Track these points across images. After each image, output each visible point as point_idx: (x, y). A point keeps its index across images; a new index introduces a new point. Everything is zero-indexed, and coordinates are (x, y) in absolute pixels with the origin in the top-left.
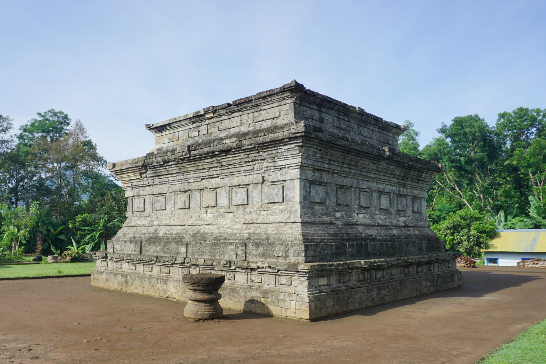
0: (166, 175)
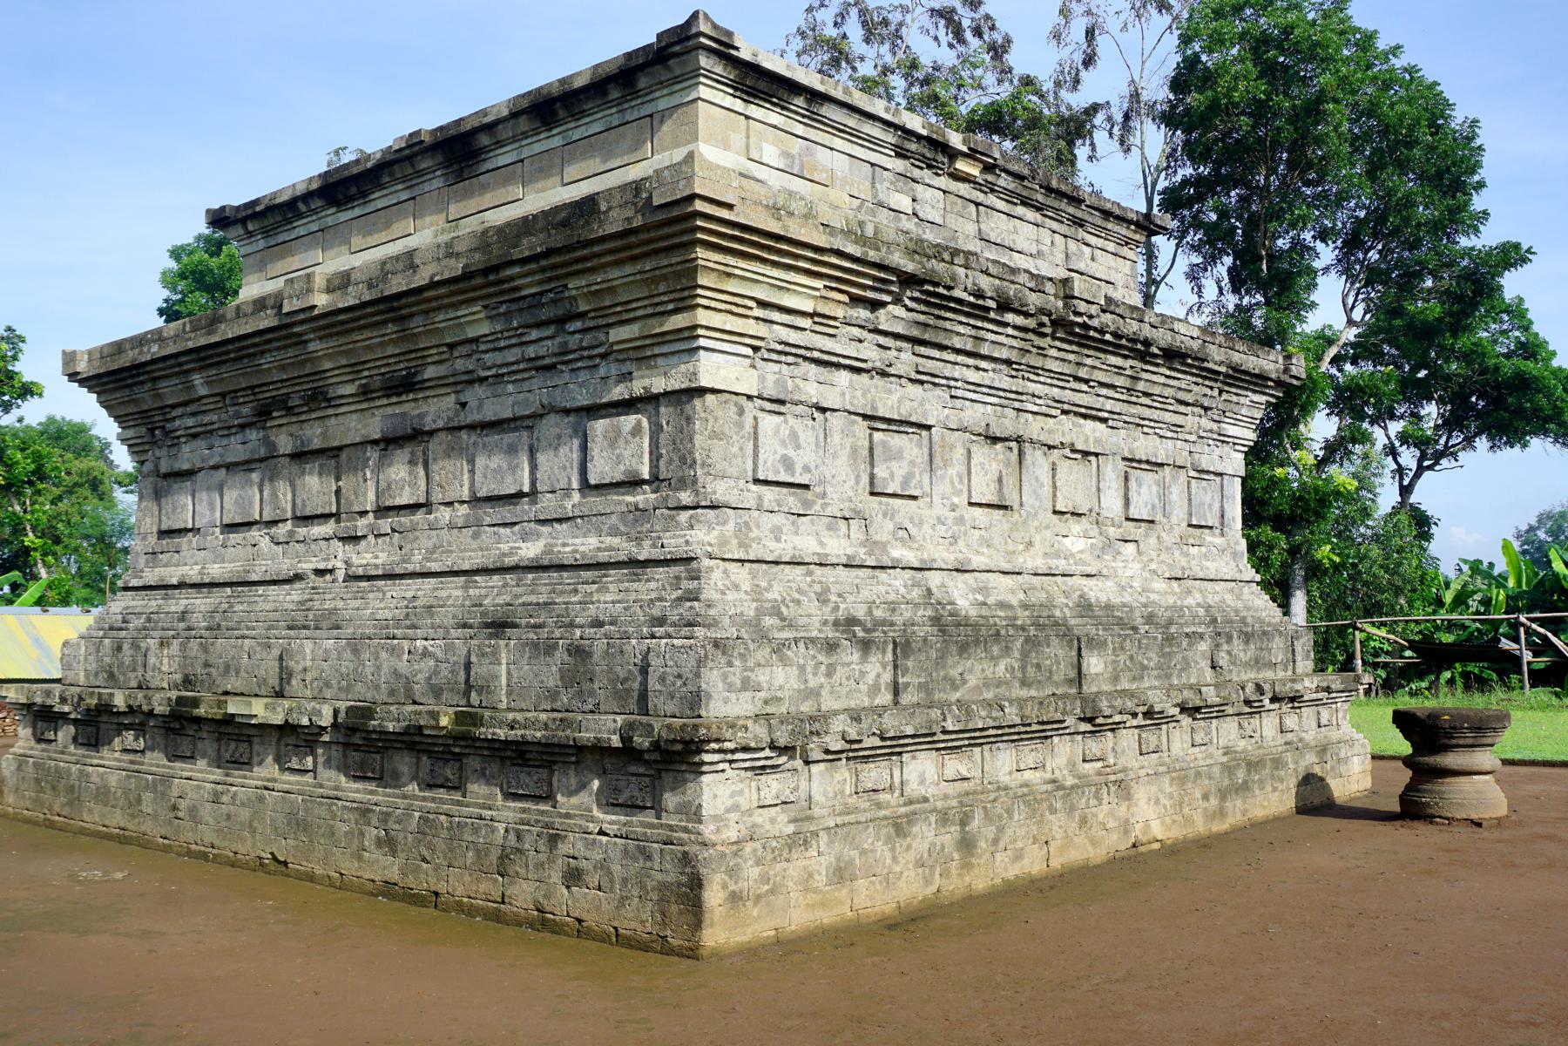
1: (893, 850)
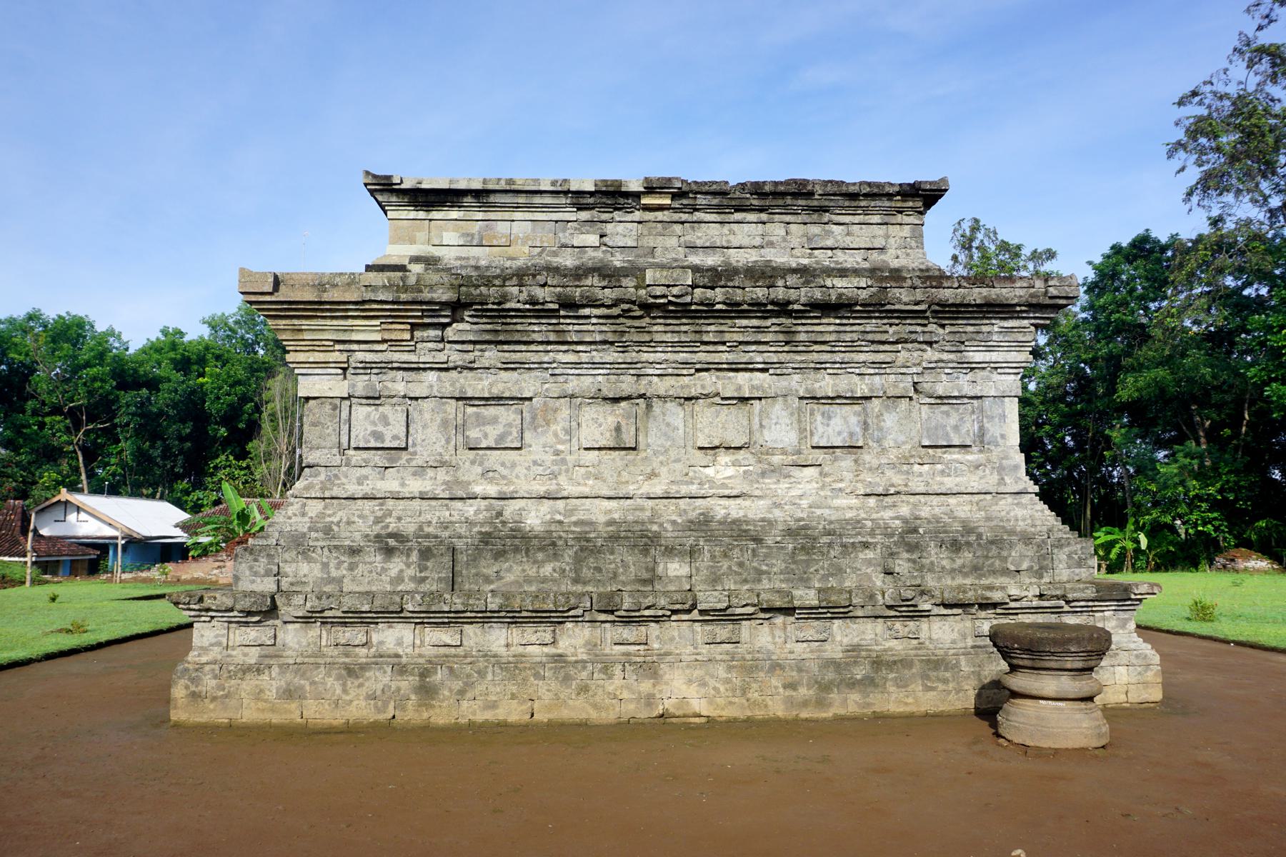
0: (542, 343)
1: (344, 685)
